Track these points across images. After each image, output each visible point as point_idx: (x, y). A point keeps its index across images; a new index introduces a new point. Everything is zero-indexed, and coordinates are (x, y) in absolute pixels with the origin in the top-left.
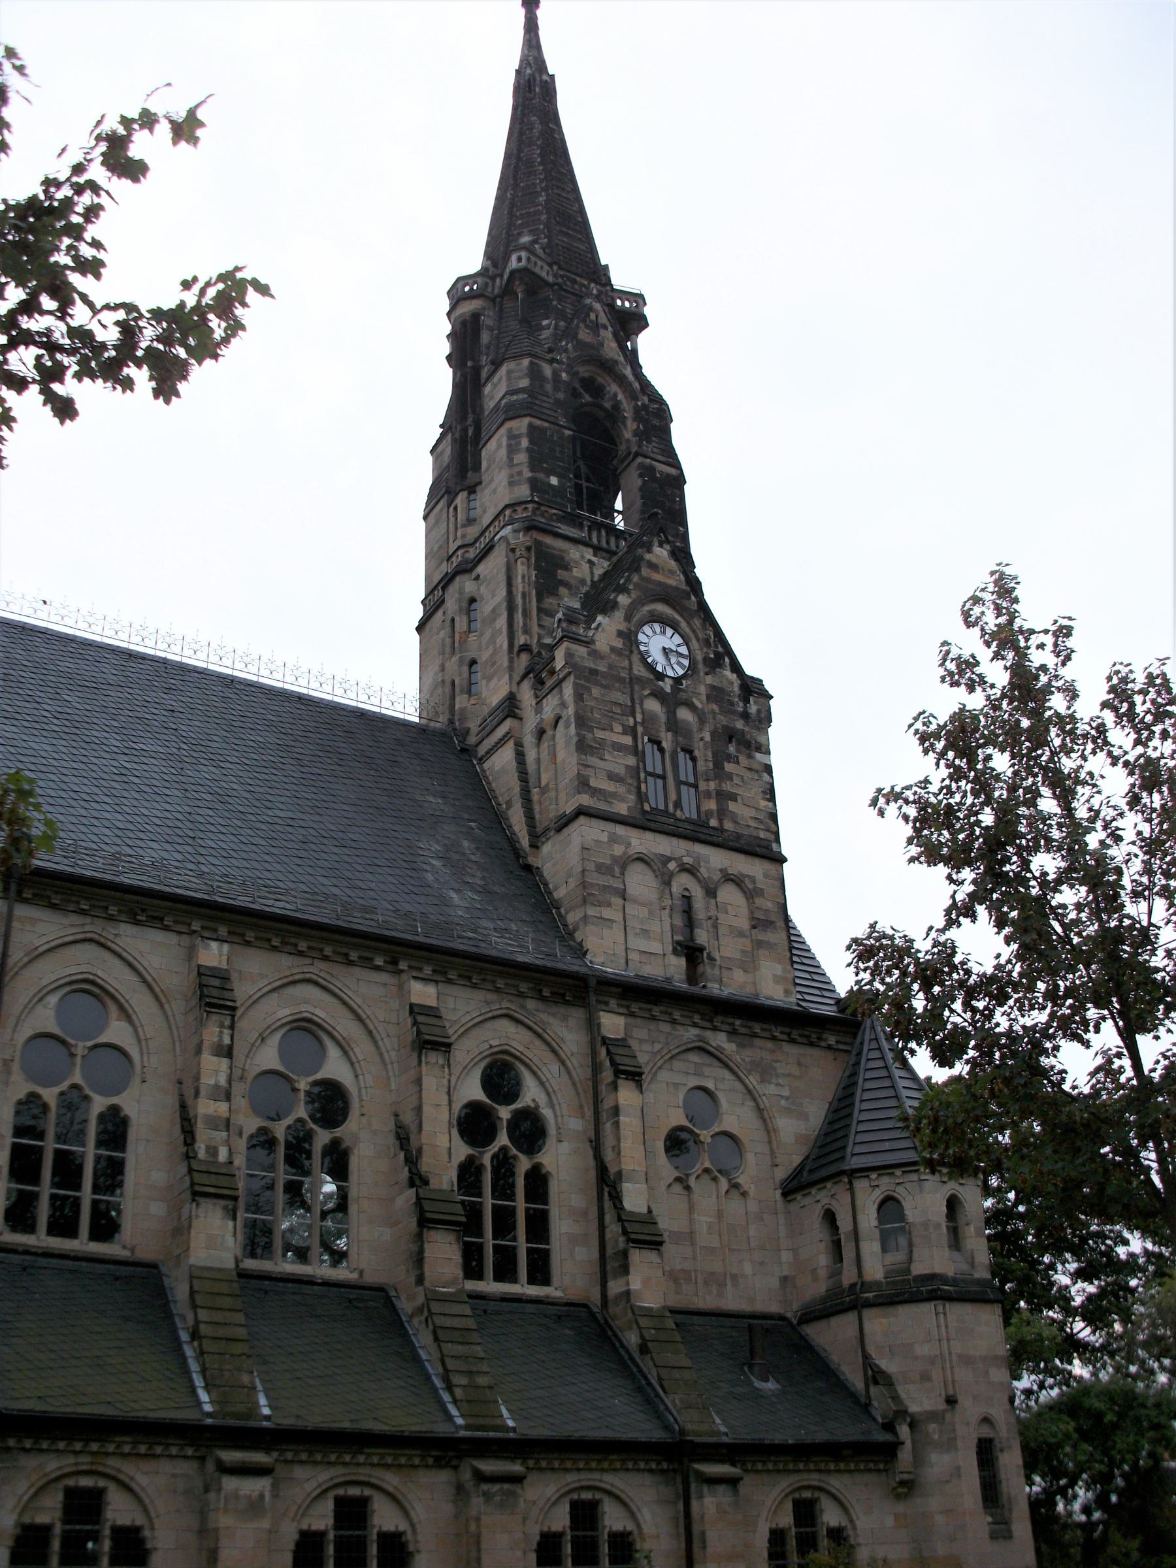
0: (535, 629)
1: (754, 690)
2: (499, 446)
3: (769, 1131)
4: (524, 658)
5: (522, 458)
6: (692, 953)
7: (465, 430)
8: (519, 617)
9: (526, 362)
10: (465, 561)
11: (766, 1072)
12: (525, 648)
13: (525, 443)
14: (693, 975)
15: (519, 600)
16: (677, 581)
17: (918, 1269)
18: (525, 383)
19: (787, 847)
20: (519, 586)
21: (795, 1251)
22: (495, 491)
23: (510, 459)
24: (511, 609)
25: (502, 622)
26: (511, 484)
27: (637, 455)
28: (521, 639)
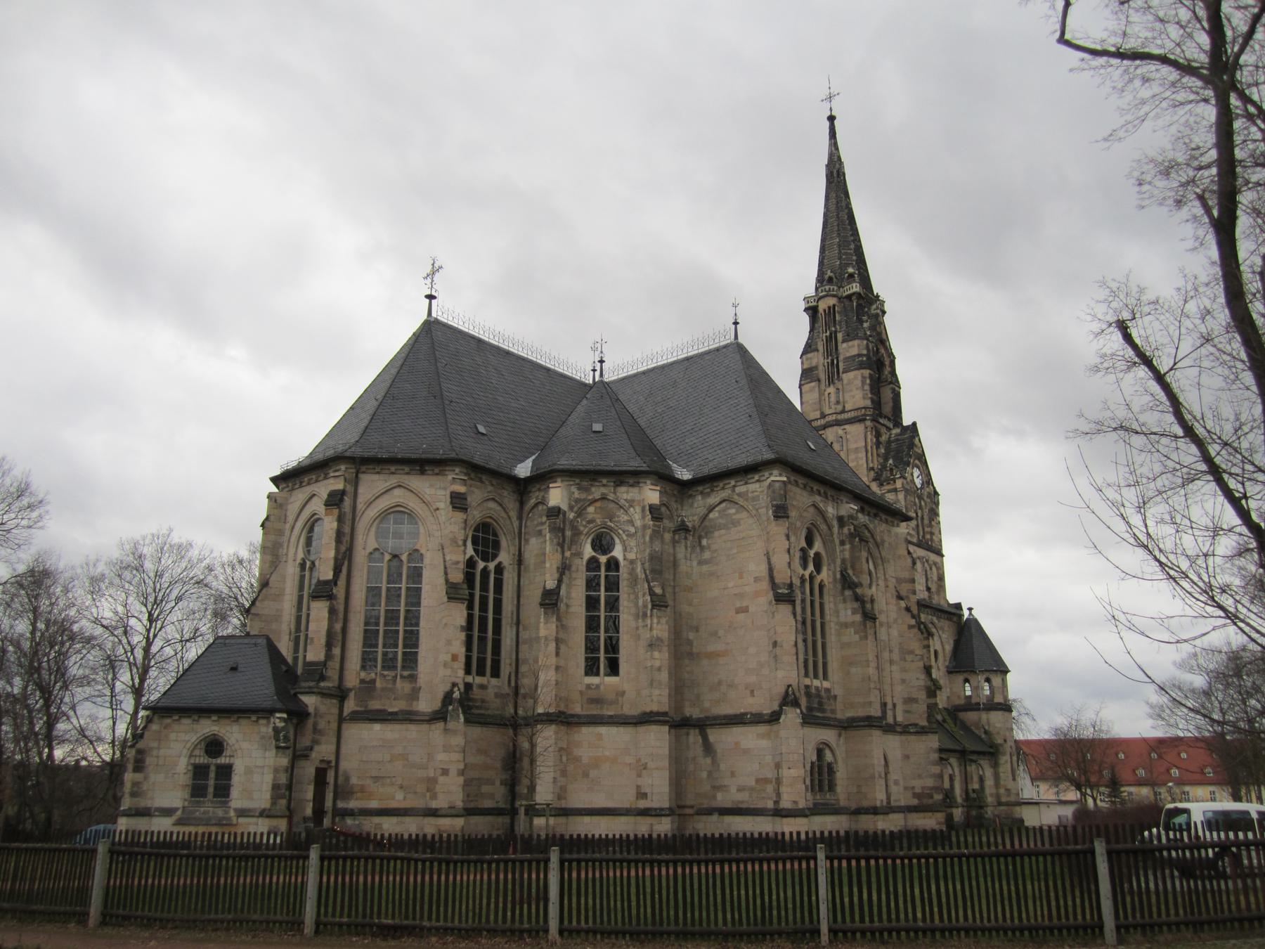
0: (875, 461)
1: (936, 493)
2: (856, 378)
3: (944, 649)
4: (872, 472)
5: (867, 387)
6: (928, 589)
7: (832, 361)
8: (869, 454)
9: (865, 342)
10: (836, 420)
11: (942, 629)
12: (872, 469)
13: (868, 381)
14: (930, 597)
15: (869, 448)
16: (920, 452)
17: (996, 700)
18: (865, 352)
19: (944, 552)
20: (869, 440)
21: (951, 689)
22: (853, 397)
23: (863, 386)
24: (867, 452)
25: (863, 455)
26: (864, 398)
27: (891, 383)
28: (871, 465)
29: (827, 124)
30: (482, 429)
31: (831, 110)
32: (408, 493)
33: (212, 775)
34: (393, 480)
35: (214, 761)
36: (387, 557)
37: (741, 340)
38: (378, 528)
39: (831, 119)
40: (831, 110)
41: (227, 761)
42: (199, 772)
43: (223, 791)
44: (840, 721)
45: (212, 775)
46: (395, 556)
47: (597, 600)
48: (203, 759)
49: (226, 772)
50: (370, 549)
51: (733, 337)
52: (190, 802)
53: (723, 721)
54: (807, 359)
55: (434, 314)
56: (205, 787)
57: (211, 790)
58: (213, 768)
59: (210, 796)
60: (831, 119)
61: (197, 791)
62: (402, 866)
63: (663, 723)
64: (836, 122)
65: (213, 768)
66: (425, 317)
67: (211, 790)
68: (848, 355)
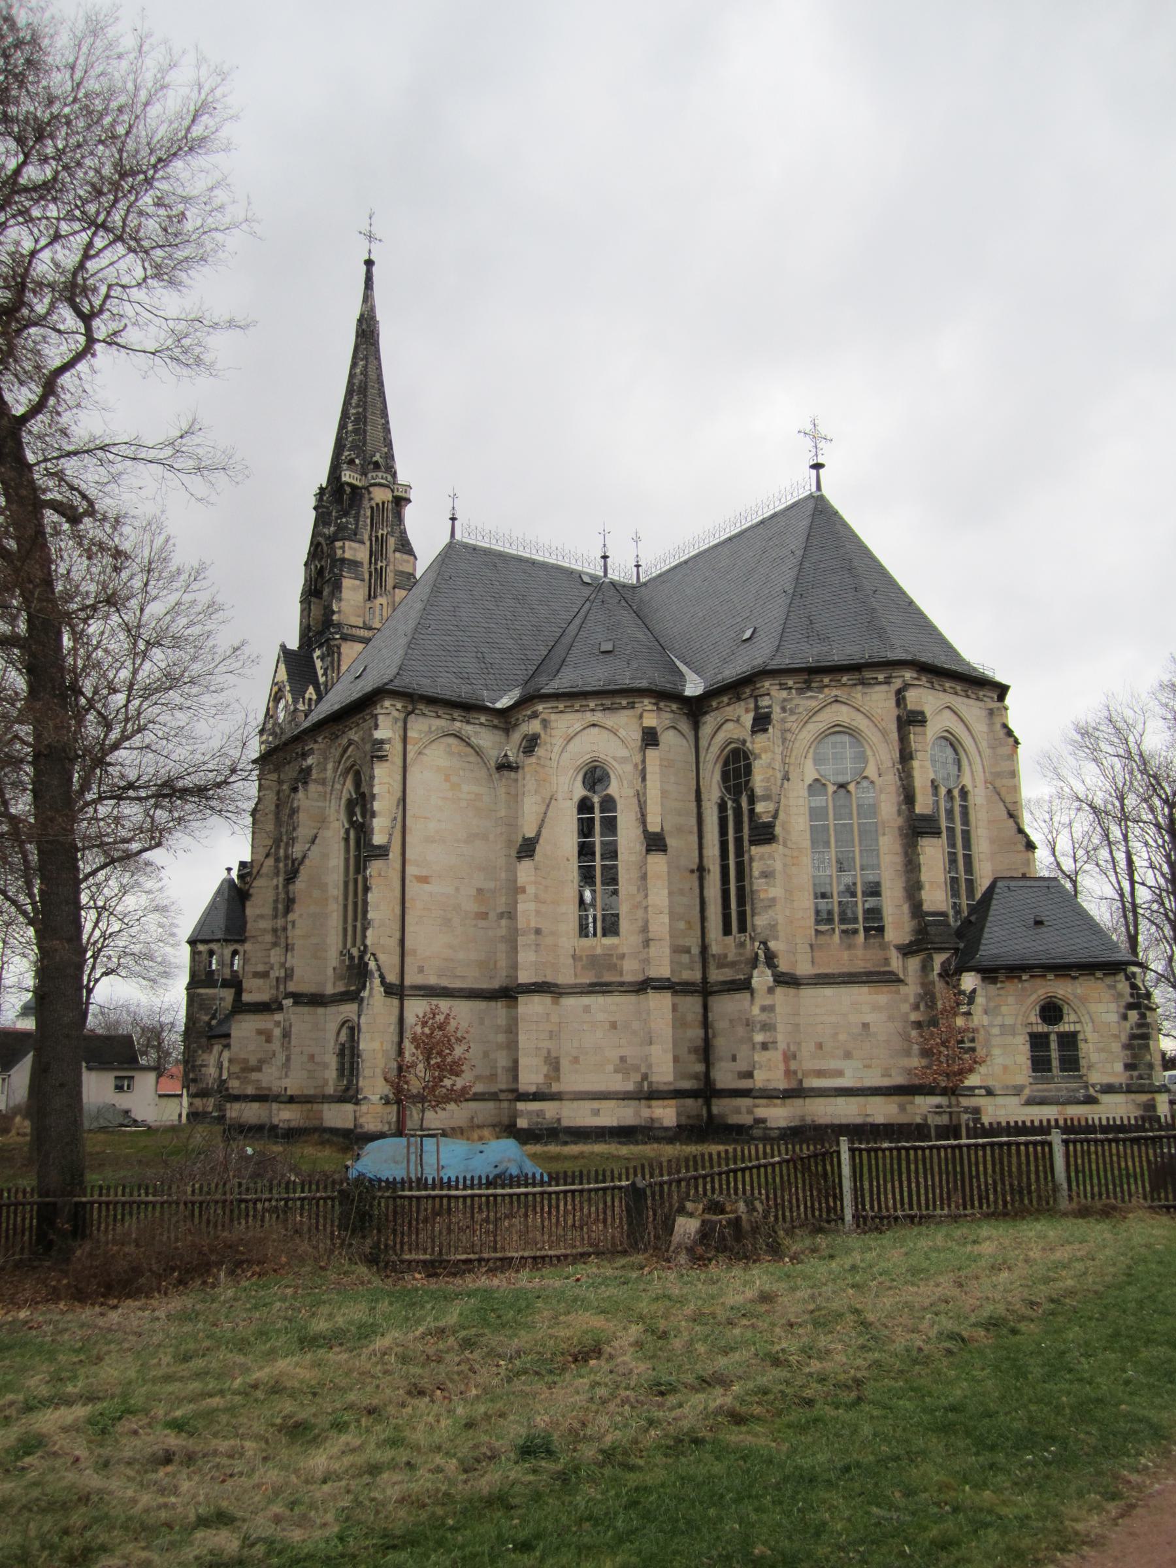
7: (376, 564)
29: (364, 268)
30: (747, 635)
31: (370, 252)
32: (955, 718)
33: (1054, 1045)
34: (589, 717)
35: (1056, 1028)
36: (831, 789)
37: (826, 492)
38: (815, 753)
39: (369, 263)
40: (370, 252)
41: (1072, 1029)
42: (1038, 1042)
43: (1071, 1063)
44: (630, 984)
45: (1054, 1045)
46: (842, 786)
47: (826, 828)
48: (1042, 1028)
49: (1070, 1041)
50: (809, 781)
51: (814, 489)
52: (1035, 1078)
53: (810, 981)
54: (351, 548)
55: (458, 536)
56: (1048, 1061)
57: (1055, 1063)
58: (1053, 1037)
59: (1056, 1071)
60: (369, 263)
61: (1040, 1064)
62: (788, 1170)
63: (692, 992)
64: (375, 269)
65: (1053, 1037)
66: (447, 539)
67: (1055, 1063)
68: (401, 568)
